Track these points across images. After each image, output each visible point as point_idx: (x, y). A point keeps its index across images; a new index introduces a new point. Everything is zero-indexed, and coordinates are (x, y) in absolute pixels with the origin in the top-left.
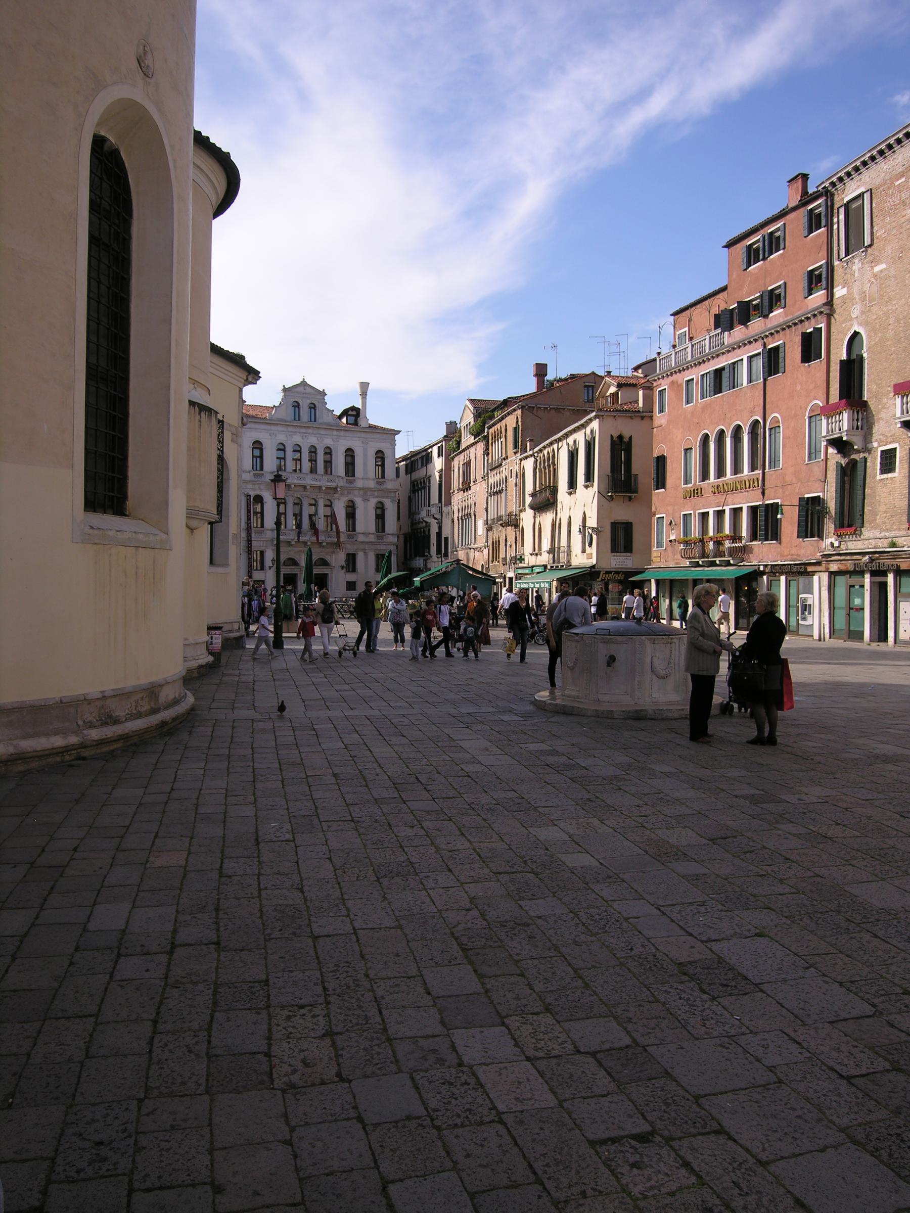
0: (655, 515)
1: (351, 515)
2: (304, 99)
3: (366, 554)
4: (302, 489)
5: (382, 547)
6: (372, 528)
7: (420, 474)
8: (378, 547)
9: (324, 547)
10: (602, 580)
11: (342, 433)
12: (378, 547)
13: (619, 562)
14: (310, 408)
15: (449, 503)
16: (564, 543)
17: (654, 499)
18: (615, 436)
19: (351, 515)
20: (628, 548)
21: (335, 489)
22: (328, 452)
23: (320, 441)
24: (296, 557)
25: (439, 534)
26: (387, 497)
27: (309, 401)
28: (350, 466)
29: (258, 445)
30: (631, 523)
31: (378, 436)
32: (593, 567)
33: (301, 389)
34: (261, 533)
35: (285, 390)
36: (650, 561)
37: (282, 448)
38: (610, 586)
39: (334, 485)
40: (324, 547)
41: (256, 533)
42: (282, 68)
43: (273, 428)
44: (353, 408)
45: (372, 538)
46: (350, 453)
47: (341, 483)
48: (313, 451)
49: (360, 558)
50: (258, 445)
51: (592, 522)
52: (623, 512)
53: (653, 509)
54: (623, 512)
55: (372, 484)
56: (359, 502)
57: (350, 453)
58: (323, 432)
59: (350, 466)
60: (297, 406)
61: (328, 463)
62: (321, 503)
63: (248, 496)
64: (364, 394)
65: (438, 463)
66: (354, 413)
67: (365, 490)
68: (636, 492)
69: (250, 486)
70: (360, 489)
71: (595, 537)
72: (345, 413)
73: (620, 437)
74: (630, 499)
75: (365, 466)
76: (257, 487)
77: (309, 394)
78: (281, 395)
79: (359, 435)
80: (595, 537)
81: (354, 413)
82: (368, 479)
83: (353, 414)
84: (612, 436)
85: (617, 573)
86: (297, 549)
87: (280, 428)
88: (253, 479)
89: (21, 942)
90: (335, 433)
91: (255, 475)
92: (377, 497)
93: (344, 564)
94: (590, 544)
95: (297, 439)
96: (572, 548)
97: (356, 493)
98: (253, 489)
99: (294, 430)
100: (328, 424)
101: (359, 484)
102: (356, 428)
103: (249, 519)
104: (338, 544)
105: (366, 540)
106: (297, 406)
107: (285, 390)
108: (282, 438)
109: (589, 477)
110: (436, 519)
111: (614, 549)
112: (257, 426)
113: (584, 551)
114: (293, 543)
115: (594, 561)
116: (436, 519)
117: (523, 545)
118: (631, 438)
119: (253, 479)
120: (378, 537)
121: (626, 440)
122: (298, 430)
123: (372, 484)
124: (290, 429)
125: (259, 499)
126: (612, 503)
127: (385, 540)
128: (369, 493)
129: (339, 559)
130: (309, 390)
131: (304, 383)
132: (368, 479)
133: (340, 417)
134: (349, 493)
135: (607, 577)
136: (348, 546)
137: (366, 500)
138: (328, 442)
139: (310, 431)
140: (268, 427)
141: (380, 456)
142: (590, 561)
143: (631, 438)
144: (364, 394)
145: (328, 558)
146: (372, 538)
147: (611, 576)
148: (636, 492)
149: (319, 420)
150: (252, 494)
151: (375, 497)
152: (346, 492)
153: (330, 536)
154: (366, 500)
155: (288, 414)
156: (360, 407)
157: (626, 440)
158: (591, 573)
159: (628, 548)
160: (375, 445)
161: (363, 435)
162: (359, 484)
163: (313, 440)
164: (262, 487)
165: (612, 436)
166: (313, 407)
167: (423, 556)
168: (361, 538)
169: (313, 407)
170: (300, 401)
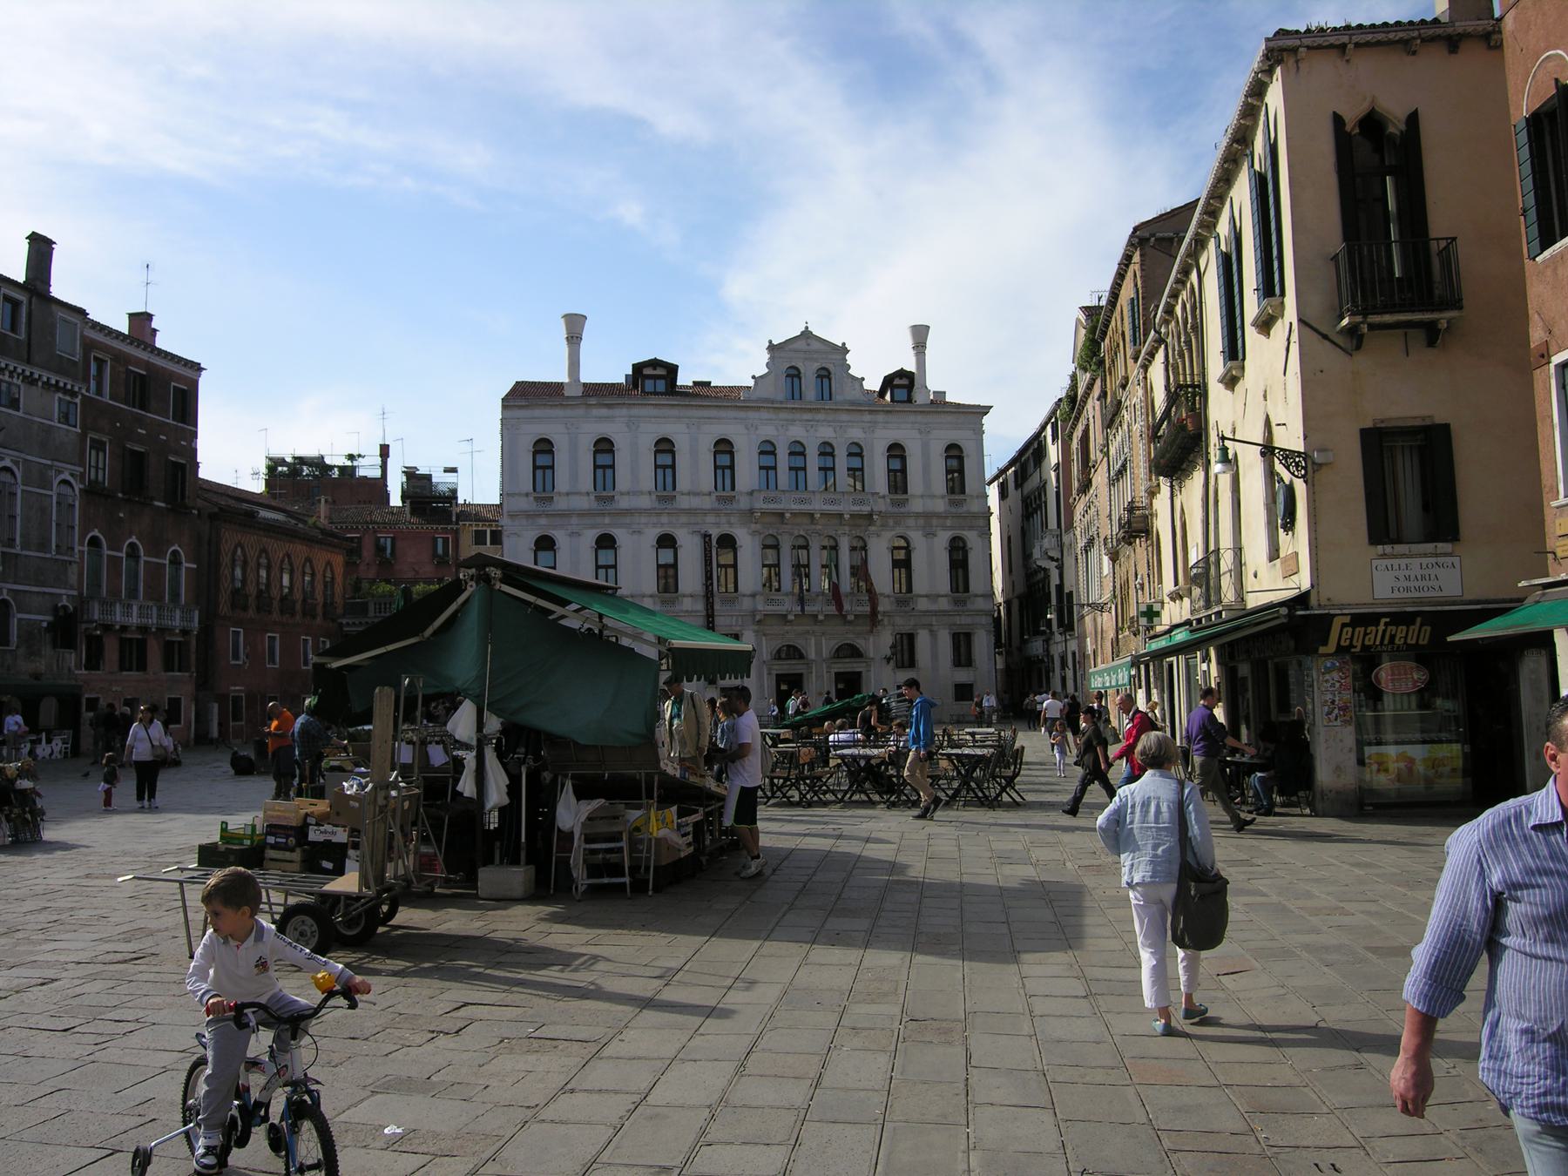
0: (1545, 356)
1: (903, 564)
2: (992, 81)
3: (933, 634)
4: (806, 520)
5: (965, 620)
6: (944, 585)
7: (1033, 483)
8: (958, 620)
9: (850, 622)
10: (1341, 650)
11: (881, 418)
12: (958, 620)
13: (1395, 578)
14: (820, 377)
15: (1070, 526)
16: (1226, 540)
17: (1537, 292)
18: (1351, 116)
19: (903, 564)
20: (1441, 522)
21: (870, 516)
22: (857, 451)
23: (841, 433)
24: (799, 643)
25: (1060, 587)
26: (971, 528)
27: (817, 365)
28: (898, 481)
29: (724, 447)
30: (1446, 428)
31: (950, 418)
32: (1302, 599)
33: (801, 345)
34: (732, 601)
35: (772, 348)
36: (1540, 555)
37: (768, 449)
38: (1385, 673)
39: (866, 509)
40: (850, 622)
41: (724, 601)
42: (961, 45)
43: (751, 414)
44: (901, 373)
45: (944, 604)
46: (896, 451)
47: (882, 506)
48: (827, 451)
49: (923, 641)
50: (724, 447)
51: (1291, 437)
52: (1404, 390)
53: (1537, 335)
54: (1404, 390)
55: (940, 506)
56: (916, 538)
57: (896, 451)
58: (844, 417)
59: (898, 481)
60: (794, 374)
61: (856, 472)
62: (844, 545)
63: (706, 537)
64: (920, 347)
65: (1053, 453)
66: (905, 382)
67: (928, 516)
68: (1457, 304)
69: (710, 519)
70: (918, 515)
71: (1300, 487)
72: (888, 382)
73: (1372, 123)
74: (1432, 335)
75: (926, 475)
76: (723, 519)
77: (816, 352)
78: (766, 357)
79: (912, 418)
80: (1300, 487)
81: (905, 382)
82: (933, 497)
83: (902, 384)
84: (1338, 120)
85: (1401, 619)
86: (800, 629)
87: (765, 415)
88: (716, 505)
89: (703, 1132)
90: (867, 417)
91: (719, 499)
92: (951, 528)
93: (888, 652)
94: (1289, 524)
95: (797, 432)
96: (1248, 556)
97: (911, 522)
98: (717, 524)
99: (789, 416)
100: (852, 403)
101: (916, 506)
102: (906, 407)
103: (708, 576)
104: (873, 618)
105: (934, 607)
106: (794, 374)
107: (772, 348)
108: (768, 432)
109: (1270, 287)
110: (1052, 559)
111: (1382, 530)
112: (722, 413)
113: (1274, 554)
114: (791, 617)
115: (1304, 581)
116: (1052, 559)
117: (1160, 582)
118: (1413, 119)
119: (716, 505)
120: (956, 602)
121: (1396, 127)
122: (798, 416)
123: (940, 506)
124: (783, 415)
125: (727, 542)
126: (1361, 361)
127: (969, 606)
128: (935, 522)
129: (879, 644)
130: (816, 345)
131: (806, 334)
132: (933, 497)
133: (882, 393)
134: (897, 523)
135: (1360, 638)
136: (899, 620)
137: (930, 535)
138: (856, 434)
139: (821, 416)
140: (742, 414)
141: (954, 453)
142: (1293, 582)
143: (1413, 119)
144: (920, 347)
145: (860, 643)
146: (944, 604)
147: (1374, 636)
148: (1457, 304)
149: (837, 397)
150: (715, 533)
151: (945, 528)
152: (891, 522)
153: (860, 603)
154: (930, 535)
155: (779, 391)
156: (913, 370)
157: (1396, 127)
158: (1297, 624)
159: (1441, 522)
160: (941, 437)
161: (919, 418)
162: (916, 506)
163: (826, 433)
164: (733, 520)
165: (1338, 120)
166: (824, 375)
167: (1038, 633)
168: (923, 604)
169: (824, 375)
170: (800, 365)
